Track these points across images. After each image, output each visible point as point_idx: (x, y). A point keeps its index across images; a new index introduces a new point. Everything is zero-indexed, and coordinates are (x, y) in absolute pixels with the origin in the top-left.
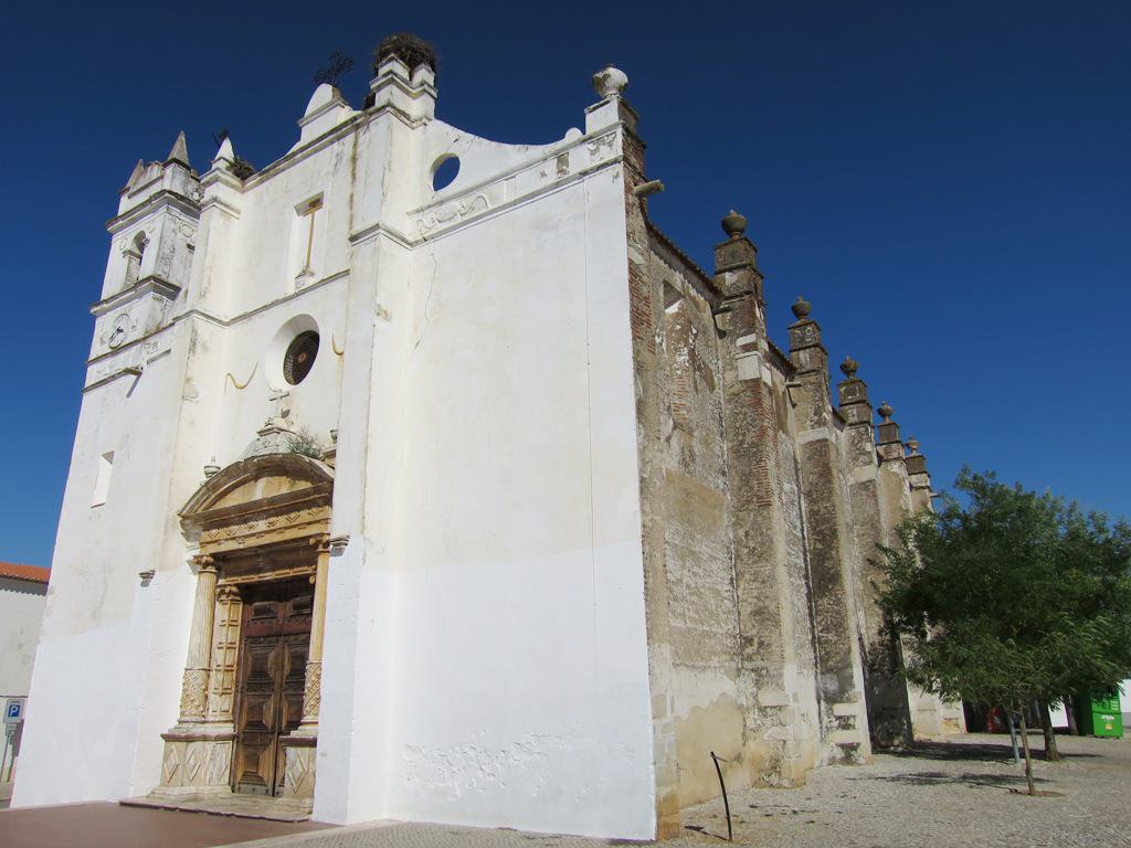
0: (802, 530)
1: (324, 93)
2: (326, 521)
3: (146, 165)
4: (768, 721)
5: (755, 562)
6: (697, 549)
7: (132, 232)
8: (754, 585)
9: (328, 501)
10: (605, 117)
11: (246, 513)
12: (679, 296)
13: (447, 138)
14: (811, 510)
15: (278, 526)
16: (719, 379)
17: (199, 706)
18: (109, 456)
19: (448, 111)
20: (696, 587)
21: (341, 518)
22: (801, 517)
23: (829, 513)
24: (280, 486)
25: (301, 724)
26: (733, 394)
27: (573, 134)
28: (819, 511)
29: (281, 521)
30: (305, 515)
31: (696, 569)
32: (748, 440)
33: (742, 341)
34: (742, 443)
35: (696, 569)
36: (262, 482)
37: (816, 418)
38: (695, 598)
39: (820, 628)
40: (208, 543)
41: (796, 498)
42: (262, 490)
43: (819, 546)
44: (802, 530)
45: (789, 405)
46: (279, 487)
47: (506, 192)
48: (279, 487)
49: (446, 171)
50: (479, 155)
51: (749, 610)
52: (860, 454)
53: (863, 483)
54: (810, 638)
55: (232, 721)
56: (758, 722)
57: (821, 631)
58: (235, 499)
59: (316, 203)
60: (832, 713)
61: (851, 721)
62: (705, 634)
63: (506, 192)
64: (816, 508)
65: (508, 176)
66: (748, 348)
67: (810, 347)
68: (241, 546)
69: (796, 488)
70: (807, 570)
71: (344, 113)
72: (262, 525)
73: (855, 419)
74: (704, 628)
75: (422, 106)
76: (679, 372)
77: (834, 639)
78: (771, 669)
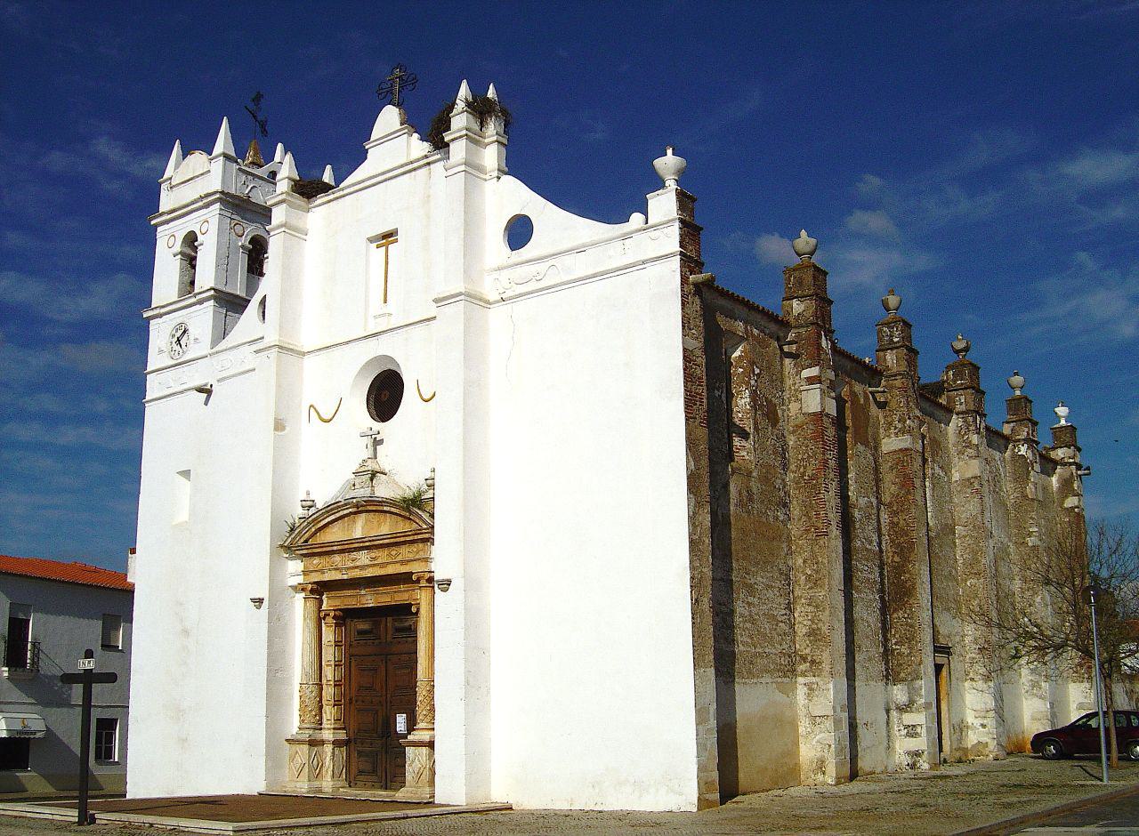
0: (880, 544)
1: (389, 118)
2: (427, 560)
3: (186, 153)
4: (817, 729)
5: (811, 588)
6: (752, 581)
7: (180, 228)
8: (810, 609)
9: (429, 541)
10: (664, 204)
11: (348, 548)
12: (742, 339)
13: (515, 196)
14: (892, 522)
15: (379, 561)
16: (783, 411)
17: (316, 716)
18: (186, 474)
19: (517, 165)
20: (750, 615)
21: (444, 558)
22: (879, 530)
23: (908, 525)
24: (379, 525)
25: (414, 730)
26: (797, 426)
27: (637, 218)
28: (898, 523)
29: (382, 556)
30: (405, 552)
31: (751, 599)
32: (809, 472)
33: (806, 373)
34: (803, 474)
35: (751, 599)
36: (361, 519)
37: (899, 426)
38: (748, 625)
39: (894, 641)
40: (312, 572)
41: (875, 511)
42: (359, 528)
43: (897, 559)
44: (880, 544)
45: (874, 409)
46: (385, 527)
47: (582, 265)
48: (385, 527)
49: (519, 232)
50: (553, 222)
51: (804, 631)
52: (966, 447)
53: (968, 480)
54: (882, 650)
55: (344, 729)
56: (809, 729)
57: (896, 644)
58: (335, 534)
59: (388, 237)
60: (902, 722)
61: (919, 730)
62: (756, 655)
63: (582, 265)
64: (895, 520)
65: (580, 250)
66: (811, 380)
67: (897, 348)
68: (345, 577)
69: (874, 500)
70: (882, 583)
71: (417, 147)
72: (363, 558)
73: (963, 408)
74: (757, 650)
75: (491, 156)
76: (740, 415)
77: (907, 652)
78: (821, 683)
